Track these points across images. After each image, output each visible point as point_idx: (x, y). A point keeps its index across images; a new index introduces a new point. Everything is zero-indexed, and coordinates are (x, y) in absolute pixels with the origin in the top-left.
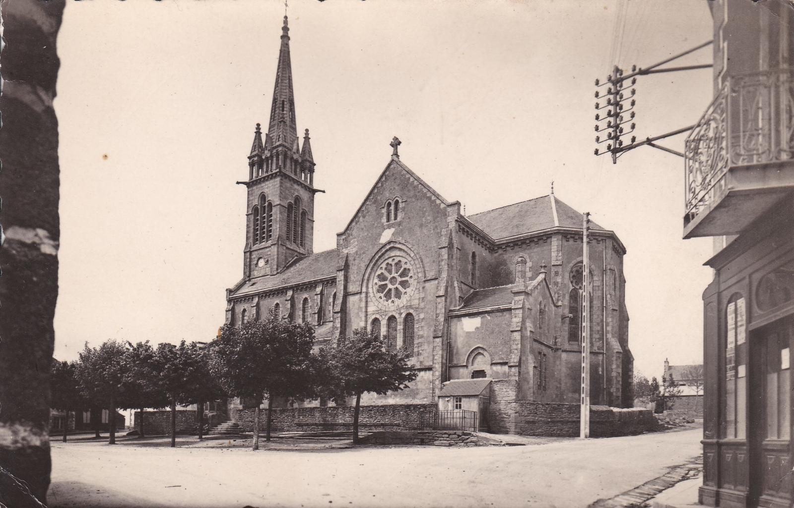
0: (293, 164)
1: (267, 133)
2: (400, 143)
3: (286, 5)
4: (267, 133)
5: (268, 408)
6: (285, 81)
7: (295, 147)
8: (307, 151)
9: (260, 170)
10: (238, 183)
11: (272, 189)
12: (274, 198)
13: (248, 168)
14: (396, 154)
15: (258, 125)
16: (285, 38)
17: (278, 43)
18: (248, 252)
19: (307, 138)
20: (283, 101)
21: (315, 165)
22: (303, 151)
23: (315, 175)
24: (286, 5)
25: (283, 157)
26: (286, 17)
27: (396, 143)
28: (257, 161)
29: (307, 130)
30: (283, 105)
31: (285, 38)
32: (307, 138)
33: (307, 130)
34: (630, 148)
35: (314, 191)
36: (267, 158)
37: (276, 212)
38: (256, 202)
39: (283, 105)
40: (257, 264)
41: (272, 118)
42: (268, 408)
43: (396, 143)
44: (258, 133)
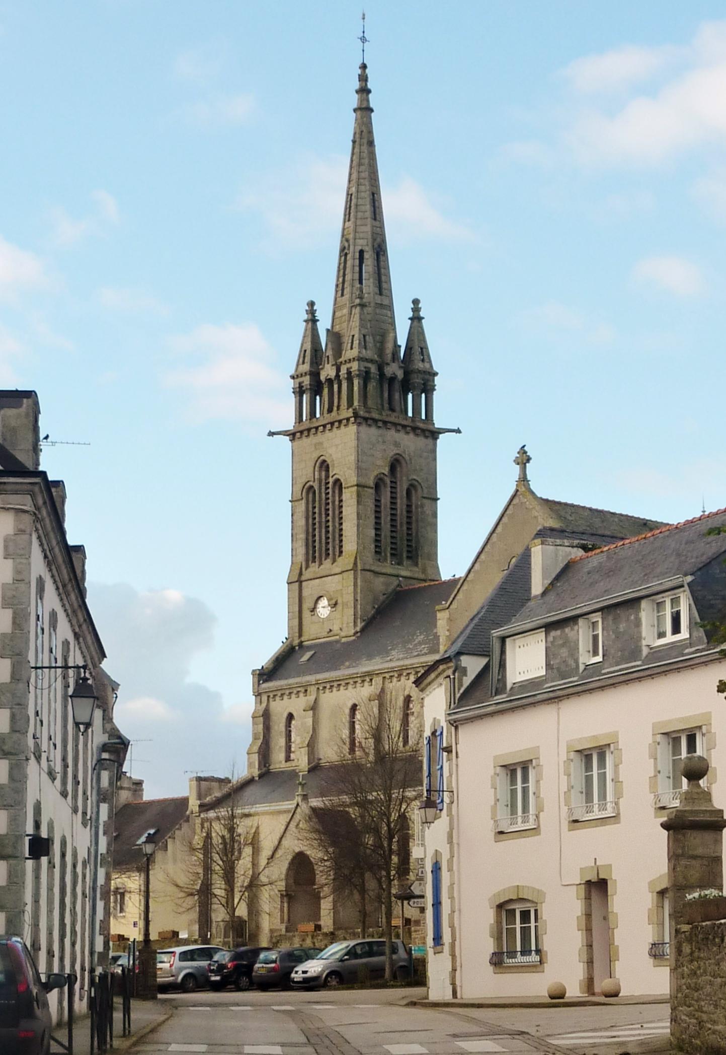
0: (386, 387)
1: (329, 328)
2: (529, 459)
3: (363, 40)
4: (329, 328)
5: (52, 1051)
6: (363, 208)
7: (389, 346)
8: (417, 350)
9: (318, 398)
10: (271, 434)
11: (343, 447)
12: (345, 469)
13: (292, 400)
14: (523, 479)
15: (312, 304)
16: (364, 110)
17: (348, 123)
18: (297, 581)
19: (416, 319)
20: (361, 252)
21: (436, 374)
22: (409, 348)
23: (436, 395)
24: (363, 40)
25: (362, 382)
26: (364, 67)
27: (523, 459)
28: (312, 384)
29: (416, 302)
30: (365, 258)
31: (364, 110)
32: (416, 319)
33: (416, 302)
34: (265, 985)
35: (434, 434)
36: (330, 381)
37: (349, 497)
38: (308, 473)
39: (365, 258)
40: (313, 610)
41: (340, 288)
42: (52, 1051)
43: (523, 459)
44: (312, 320)
